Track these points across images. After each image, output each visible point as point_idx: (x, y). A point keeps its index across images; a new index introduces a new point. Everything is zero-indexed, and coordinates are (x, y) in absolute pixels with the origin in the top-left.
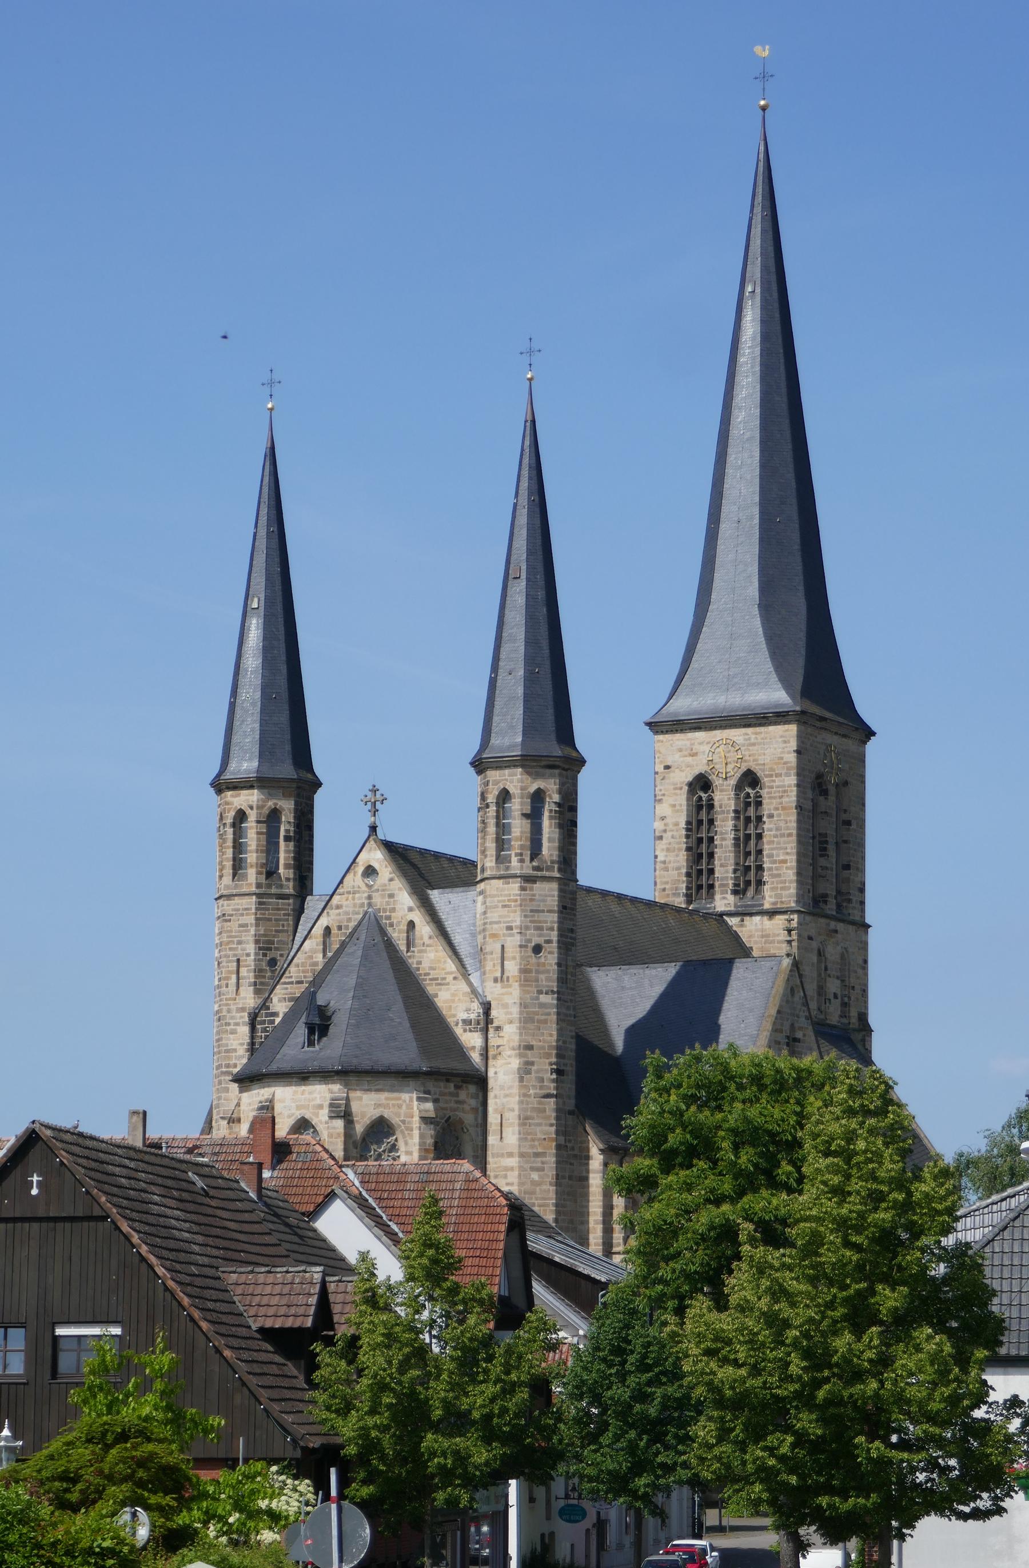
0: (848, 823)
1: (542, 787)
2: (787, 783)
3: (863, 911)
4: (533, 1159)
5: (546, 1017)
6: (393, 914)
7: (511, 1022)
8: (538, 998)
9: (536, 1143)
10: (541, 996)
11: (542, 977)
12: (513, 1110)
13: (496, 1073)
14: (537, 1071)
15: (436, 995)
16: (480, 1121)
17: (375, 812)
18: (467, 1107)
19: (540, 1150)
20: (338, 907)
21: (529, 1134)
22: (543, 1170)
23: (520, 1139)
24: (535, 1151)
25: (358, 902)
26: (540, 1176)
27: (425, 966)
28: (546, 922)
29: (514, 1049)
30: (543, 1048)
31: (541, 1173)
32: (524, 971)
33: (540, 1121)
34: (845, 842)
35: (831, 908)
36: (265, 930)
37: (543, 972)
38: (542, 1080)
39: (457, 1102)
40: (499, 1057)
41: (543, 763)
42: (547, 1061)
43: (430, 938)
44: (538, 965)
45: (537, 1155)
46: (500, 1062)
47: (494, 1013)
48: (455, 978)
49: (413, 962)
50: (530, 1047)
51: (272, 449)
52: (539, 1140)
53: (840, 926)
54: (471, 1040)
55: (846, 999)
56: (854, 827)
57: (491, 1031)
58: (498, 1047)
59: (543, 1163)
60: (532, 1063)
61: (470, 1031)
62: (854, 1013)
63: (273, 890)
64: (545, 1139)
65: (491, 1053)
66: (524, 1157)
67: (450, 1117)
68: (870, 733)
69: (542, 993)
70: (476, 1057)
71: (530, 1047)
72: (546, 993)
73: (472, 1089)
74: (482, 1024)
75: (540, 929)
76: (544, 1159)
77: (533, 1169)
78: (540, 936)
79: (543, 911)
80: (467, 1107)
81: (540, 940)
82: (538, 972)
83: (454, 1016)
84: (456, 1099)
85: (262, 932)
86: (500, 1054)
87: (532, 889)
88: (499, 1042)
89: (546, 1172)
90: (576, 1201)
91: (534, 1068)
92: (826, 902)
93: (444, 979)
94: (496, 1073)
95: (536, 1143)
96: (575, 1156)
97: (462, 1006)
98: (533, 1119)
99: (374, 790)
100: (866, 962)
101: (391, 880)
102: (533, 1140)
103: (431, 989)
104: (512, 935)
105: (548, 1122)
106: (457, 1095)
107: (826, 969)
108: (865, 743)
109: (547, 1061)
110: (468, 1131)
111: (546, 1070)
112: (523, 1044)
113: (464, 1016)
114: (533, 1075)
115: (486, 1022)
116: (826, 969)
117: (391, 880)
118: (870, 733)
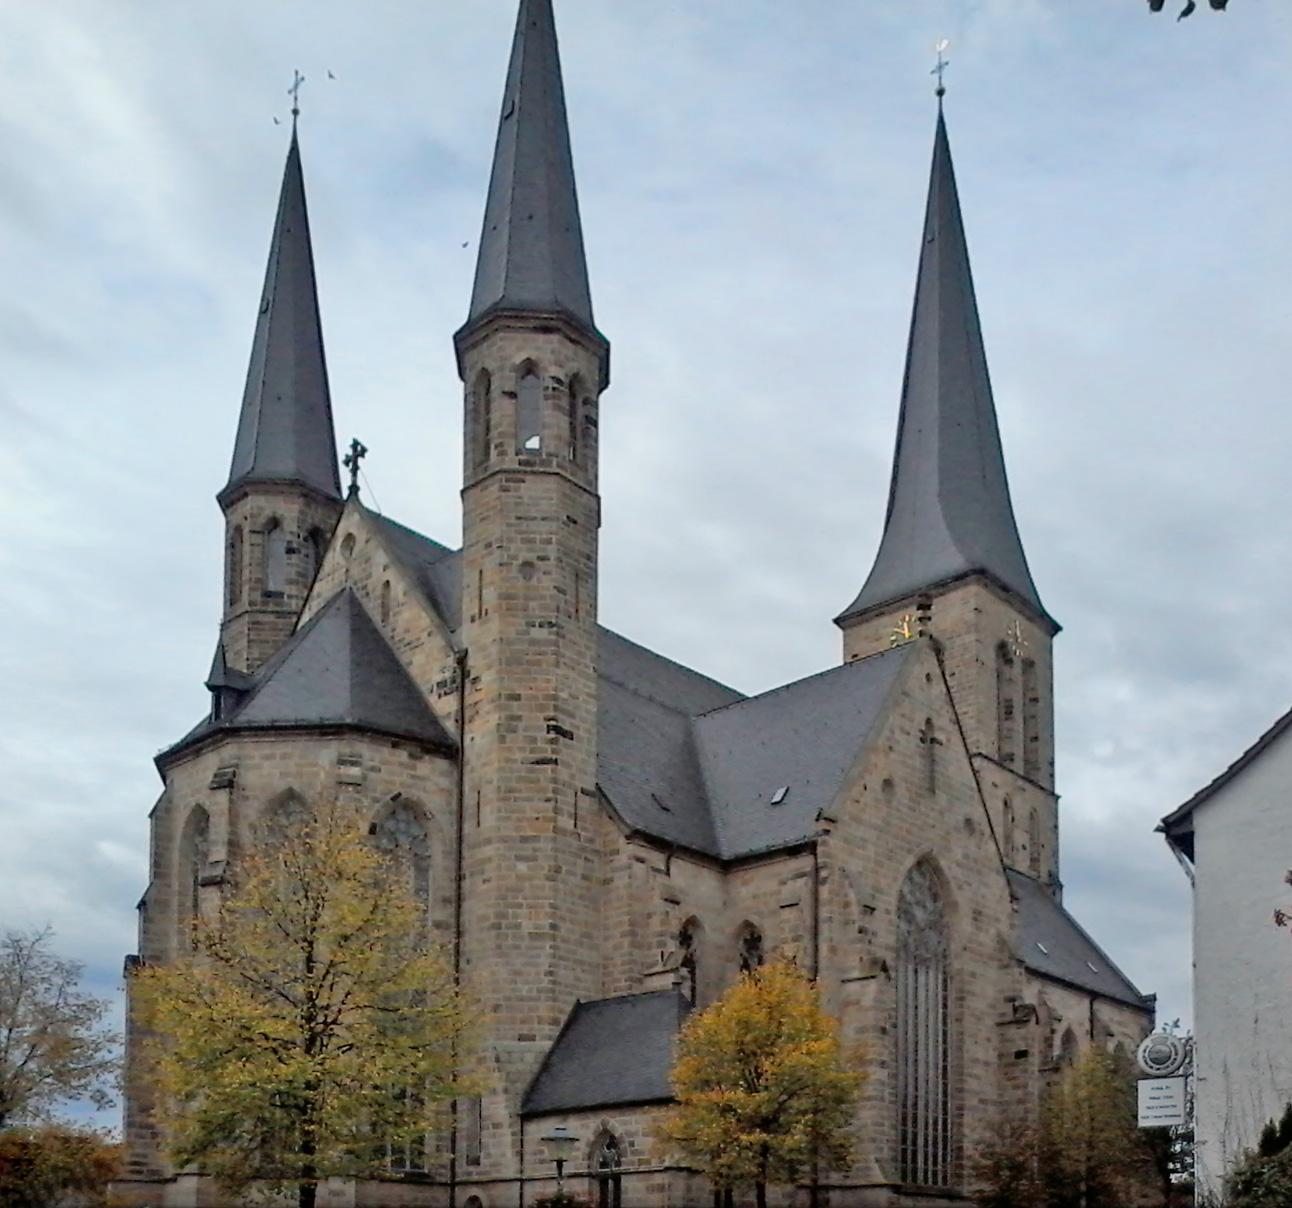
0: (1035, 700)
1: (533, 358)
2: (967, 640)
3: (1053, 783)
4: (520, 845)
5: (539, 657)
6: (369, 581)
7: (489, 667)
8: (527, 633)
9: (525, 824)
10: (533, 629)
11: (532, 604)
12: (490, 782)
13: (472, 739)
14: (526, 729)
15: (411, 663)
16: (454, 806)
17: (355, 471)
18: (429, 785)
19: (530, 833)
20: (319, 596)
21: (513, 812)
22: (535, 859)
23: (499, 819)
24: (522, 834)
25: (336, 581)
26: (529, 868)
27: (399, 633)
28: (541, 533)
29: (493, 701)
30: (535, 698)
31: (531, 863)
32: (506, 597)
33: (530, 795)
34: (1033, 717)
35: (1018, 766)
36: (260, 654)
37: (533, 599)
38: (534, 740)
39: (413, 777)
40: (476, 718)
41: (533, 323)
42: (541, 716)
43: (405, 594)
44: (528, 588)
45: (524, 839)
46: (478, 722)
47: (471, 662)
48: (429, 635)
49: (386, 633)
50: (517, 698)
51: (295, 141)
52: (528, 820)
53: (1027, 786)
54: (444, 706)
55: (1036, 855)
56: (1041, 704)
57: (468, 685)
58: (476, 703)
59: (535, 850)
60: (519, 718)
61: (446, 694)
62: (1044, 870)
63: (271, 607)
64: (537, 819)
65: (468, 714)
66: (505, 842)
67: (400, 794)
68: (1056, 628)
69: (534, 626)
70: (450, 726)
71: (517, 698)
72: (541, 626)
73: (442, 764)
74: (459, 680)
75: (531, 541)
76: (537, 845)
77: (519, 858)
78: (530, 550)
79: (535, 518)
80: (429, 785)
81: (532, 556)
82: (527, 598)
83: (428, 681)
84: (413, 772)
85: (256, 656)
86: (477, 712)
87: (517, 490)
88: (477, 697)
89: (540, 861)
90: (596, 910)
91: (521, 725)
92: (1012, 760)
93: (418, 639)
94: (472, 739)
95: (525, 824)
96: (597, 852)
97: (436, 667)
98: (520, 791)
99: (356, 444)
100: (1056, 827)
101: (367, 541)
102: (519, 820)
103: (404, 659)
104: (490, 554)
105: (542, 795)
106: (414, 768)
107: (1013, 819)
108: (1052, 636)
109: (541, 716)
110: (433, 816)
111: (539, 728)
112: (504, 692)
113: (438, 678)
114: (521, 733)
115: (462, 677)
116: (1013, 819)
117: (367, 541)
118: (1056, 628)
